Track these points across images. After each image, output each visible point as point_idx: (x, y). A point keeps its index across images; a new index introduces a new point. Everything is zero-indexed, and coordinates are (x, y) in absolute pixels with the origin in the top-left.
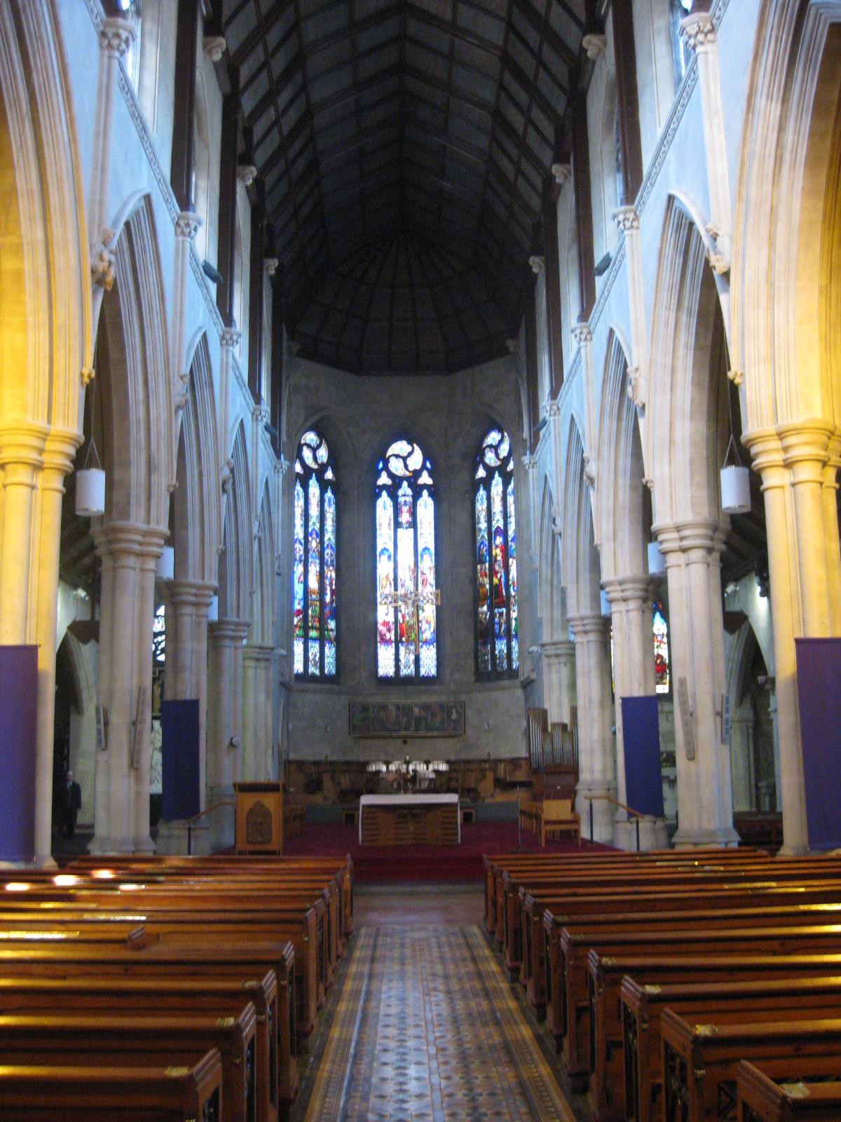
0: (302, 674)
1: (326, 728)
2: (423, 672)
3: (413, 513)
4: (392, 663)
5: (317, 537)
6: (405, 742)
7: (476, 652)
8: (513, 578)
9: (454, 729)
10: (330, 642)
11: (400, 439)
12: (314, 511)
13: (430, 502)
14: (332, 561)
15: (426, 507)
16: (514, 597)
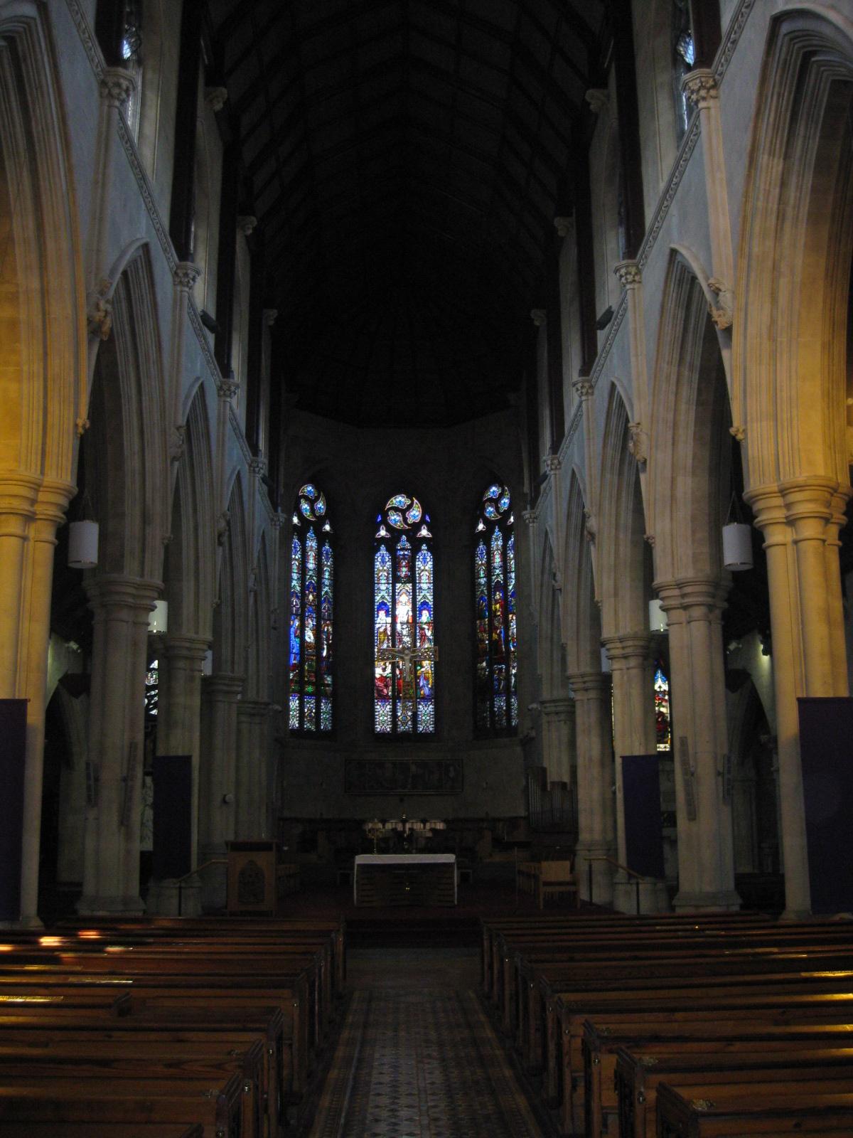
3: (412, 568)
4: (389, 718)
6: (402, 800)
8: (513, 633)
12: (311, 565)
13: (429, 557)
14: (329, 615)
15: (425, 566)
16: (513, 652)
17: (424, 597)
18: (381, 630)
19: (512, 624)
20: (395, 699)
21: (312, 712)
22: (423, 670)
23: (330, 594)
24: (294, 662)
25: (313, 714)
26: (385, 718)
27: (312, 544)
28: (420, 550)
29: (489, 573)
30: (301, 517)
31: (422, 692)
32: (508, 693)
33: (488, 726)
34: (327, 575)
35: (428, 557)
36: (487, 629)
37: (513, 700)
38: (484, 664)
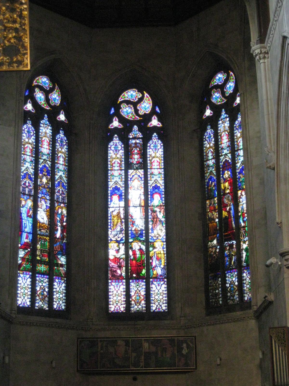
0: (28, 307)
1: (52, 363)
2: (154, 307)
3: (144, 155)
4: (122, 298)
5: (48, 174)
6: (135, 379)
7: (207, 285)
8: (242, 209)
9: (186, 364)
10: (59, 276)
11: (131, 87)
12: (45, 149)
13: (159, 143)
14: (63, 199)
15: (156, 151)
16: (244, 227)
17: (156, 181)
18: (115, 213)
19: (241, 200)
20: (128, 279)
21: (44, 290)
22: (155, 250)
23: (65, 179)
24: (26, 241)
25: (45, 293)
26: (119, 298)
27: (46, 130)
28: (150, 138)
29: (217, 156)
30: (35, 104)
31: (155, 272)
32: (239, 267)
33: (221, 302)
34: (61, 161)
35: (159, 145)
36: (217, 207)
37: (245, 275)
38: (215, 242)
